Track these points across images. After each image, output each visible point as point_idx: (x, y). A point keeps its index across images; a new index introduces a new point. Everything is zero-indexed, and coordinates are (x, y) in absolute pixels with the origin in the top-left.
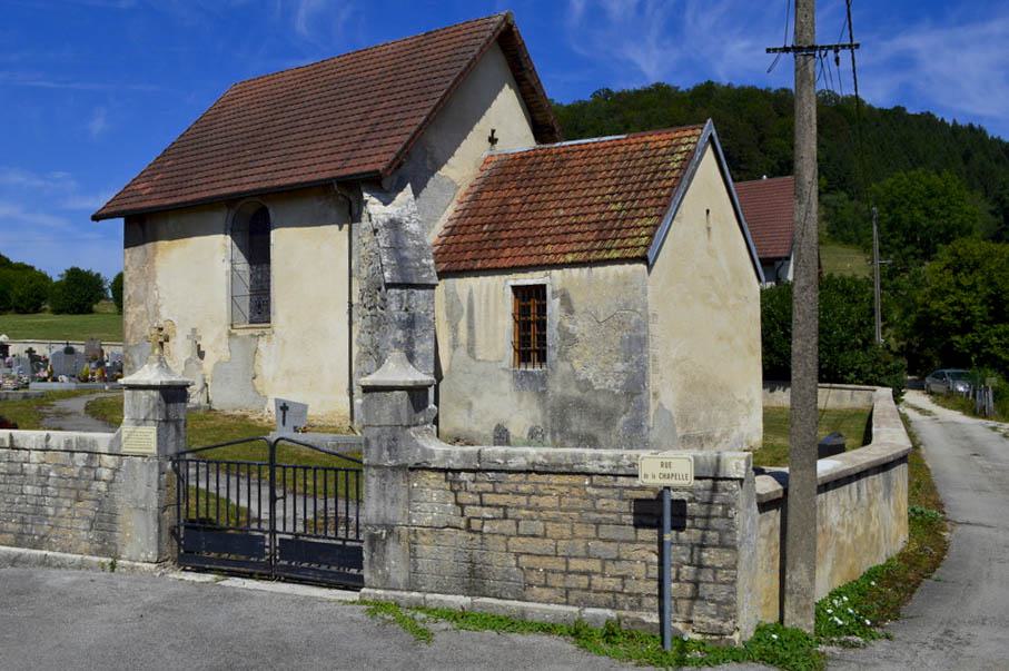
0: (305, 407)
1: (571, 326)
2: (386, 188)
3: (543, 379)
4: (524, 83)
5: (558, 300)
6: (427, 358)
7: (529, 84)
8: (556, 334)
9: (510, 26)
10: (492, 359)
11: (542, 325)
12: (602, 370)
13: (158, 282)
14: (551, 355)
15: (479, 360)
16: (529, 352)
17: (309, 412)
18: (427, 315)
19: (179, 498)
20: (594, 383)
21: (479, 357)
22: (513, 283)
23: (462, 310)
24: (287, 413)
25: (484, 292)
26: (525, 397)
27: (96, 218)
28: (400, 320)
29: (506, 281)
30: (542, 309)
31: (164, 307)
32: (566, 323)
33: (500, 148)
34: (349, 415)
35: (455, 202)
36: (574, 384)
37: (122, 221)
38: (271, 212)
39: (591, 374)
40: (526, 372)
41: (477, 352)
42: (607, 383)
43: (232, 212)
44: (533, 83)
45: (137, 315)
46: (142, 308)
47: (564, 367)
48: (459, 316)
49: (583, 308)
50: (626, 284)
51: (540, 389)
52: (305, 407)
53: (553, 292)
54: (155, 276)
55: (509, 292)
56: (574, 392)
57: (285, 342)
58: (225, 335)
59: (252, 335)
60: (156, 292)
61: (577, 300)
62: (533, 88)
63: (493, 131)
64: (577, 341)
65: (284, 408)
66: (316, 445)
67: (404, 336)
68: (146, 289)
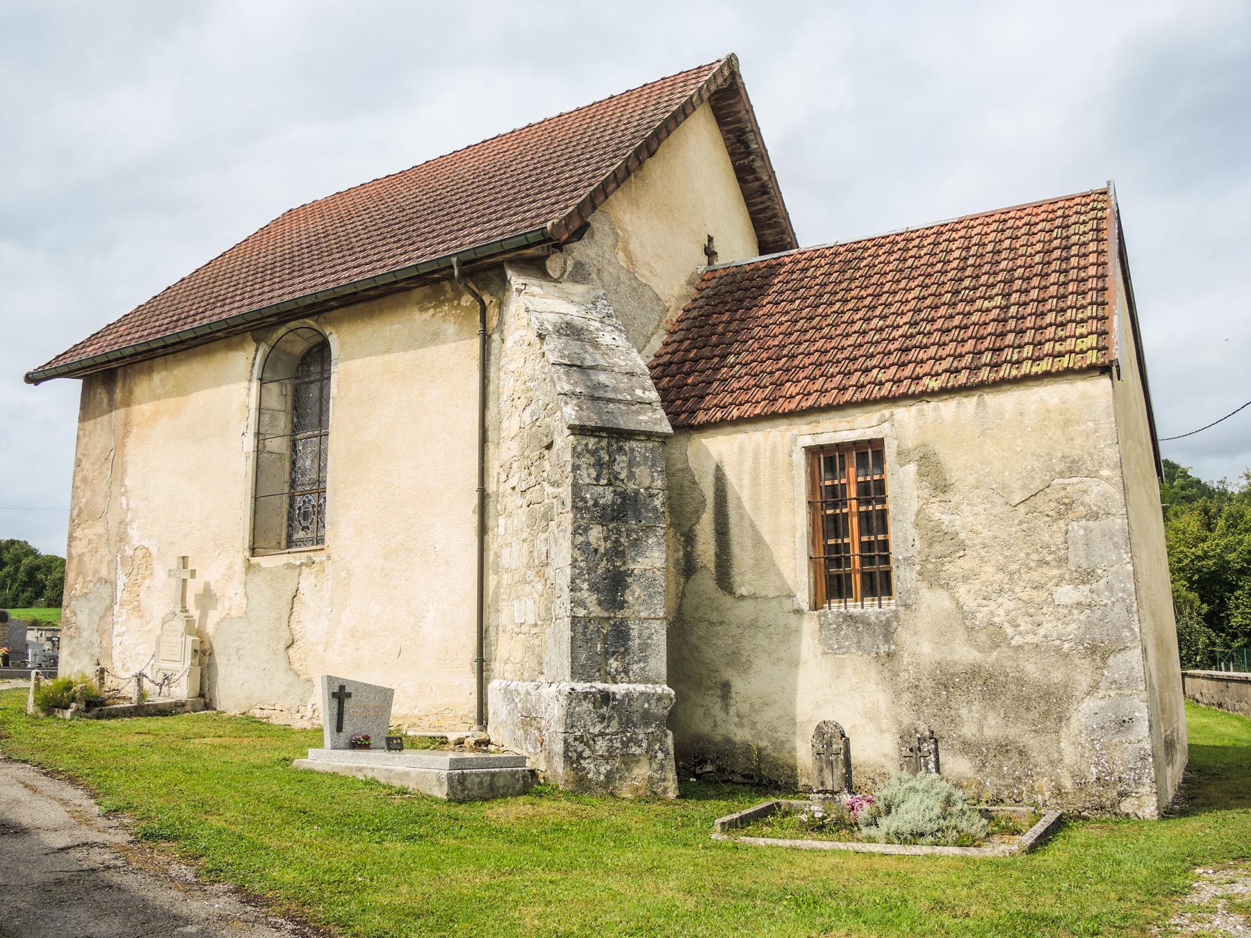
0: (386, 695)
1: (946, 518)
2: (555, 274)
3: (887, 630)
4: (750, 177)
5: (912, 468)
6: (651, 585)
7: (758, 179)
8: (913, 533)
9: (734, 75)
10: (771, 594)
11: (876, 522)
12: (1027, 603)
13: (128, 482)
14: (902, 577)
15: (742, 597)
16: (873, 557)
17: (396, 710)
18: (651, 496)
19: (1211, 678)
20: (1009, 630)
21: (744, 591)
22: (809, 441)
23: (704, 502)
24: (348, 704)
25: (748, 463)
26: (848, 670)
27: (33, 378)
28: (596, 504)
29: (794, 440)
30: (874, 492)
31: (135, 525)
32: (935, 511)
33: (722, 261)
34: (475, 714)
35: (662, 332)
36: (961, 635)
37: (74, 386)
38: (334, 341)
39: (1001, 612)
40: (849, 618)
41: (737, 579)
42: (1042, 631)
43: (264, 348)
44: (765, 178)
45: (90, 542)
46: (99, 528)
47: (933, 602)
48: (698, 513)
49: (972, 479)
50: (1067, 423)
51: (883, 649)
52: (386, 695)
53: (899, 454)
54: (124, 471)
55: (800, 458)
56: (964, 654)
57: (350, 575)
58: (239, 566)
59: (290, 566)
60: (124, 500)
61: (956, 464)
62: (764, 186)
63: (710, 239)
64: (962, 546)
65: (340, 695)
66: (654, 168)
67: (606, 539)
68: (109, 496)
